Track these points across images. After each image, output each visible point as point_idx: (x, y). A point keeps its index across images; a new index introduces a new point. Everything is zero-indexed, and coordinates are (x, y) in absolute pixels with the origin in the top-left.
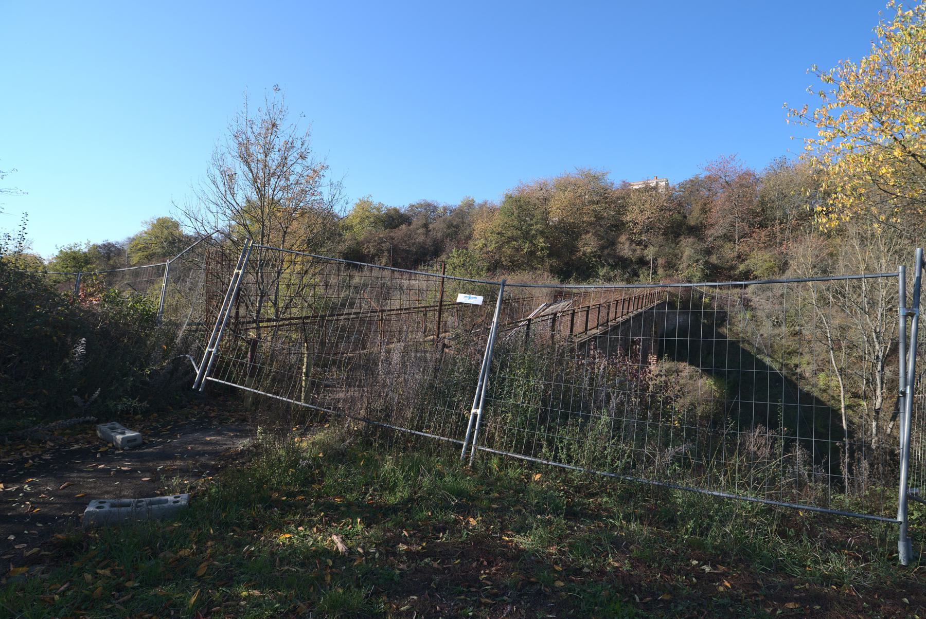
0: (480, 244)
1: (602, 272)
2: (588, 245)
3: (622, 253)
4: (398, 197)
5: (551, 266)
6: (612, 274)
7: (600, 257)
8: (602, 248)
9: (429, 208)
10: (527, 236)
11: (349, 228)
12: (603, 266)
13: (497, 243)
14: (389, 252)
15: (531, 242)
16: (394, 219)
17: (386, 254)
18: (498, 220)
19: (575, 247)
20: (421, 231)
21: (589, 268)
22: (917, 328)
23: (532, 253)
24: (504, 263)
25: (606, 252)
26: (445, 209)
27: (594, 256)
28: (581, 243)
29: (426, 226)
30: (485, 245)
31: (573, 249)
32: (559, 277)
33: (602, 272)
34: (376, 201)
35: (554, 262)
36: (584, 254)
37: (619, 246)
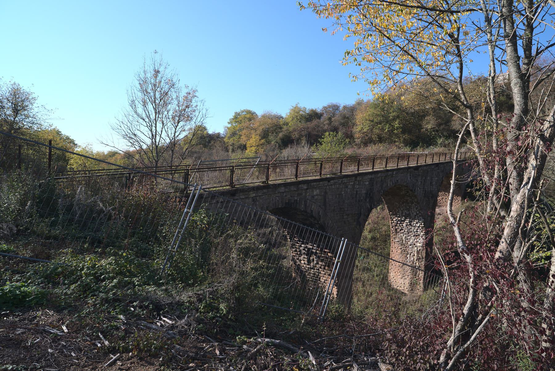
0: (359, 128)
1: (440, 141)
2: (429, 124)
3: (454, 127)
4: (315, 103)
5: (404, 139)
6: (447, 142)
7: (437, 131)
8: (439, 125)
9: (335, 107)
10: (387, 120)
11: (287, 124)
12: (440, 137)
13: (369, 126)
14: (306, 137)
15: (390, 124)
16: (314, 115)
17: (304, 138)
18: (371, 111)
19: (421, 125)
20: (327, 122)
21: (431, 139)
22: (462, 88)
23: (391, 132)
24: (374, 139)
25: (442, 127)
26: (345, 107)
27: (434, 131)
28: (424, 123)
29: (330, 119)
30: (362, 129)
31: (420, 127)
32: (410, 147)
33: (440, 141)
34: (302, 105)
35: (406, 136)
36: (427, 130)
37: (453, 123)
